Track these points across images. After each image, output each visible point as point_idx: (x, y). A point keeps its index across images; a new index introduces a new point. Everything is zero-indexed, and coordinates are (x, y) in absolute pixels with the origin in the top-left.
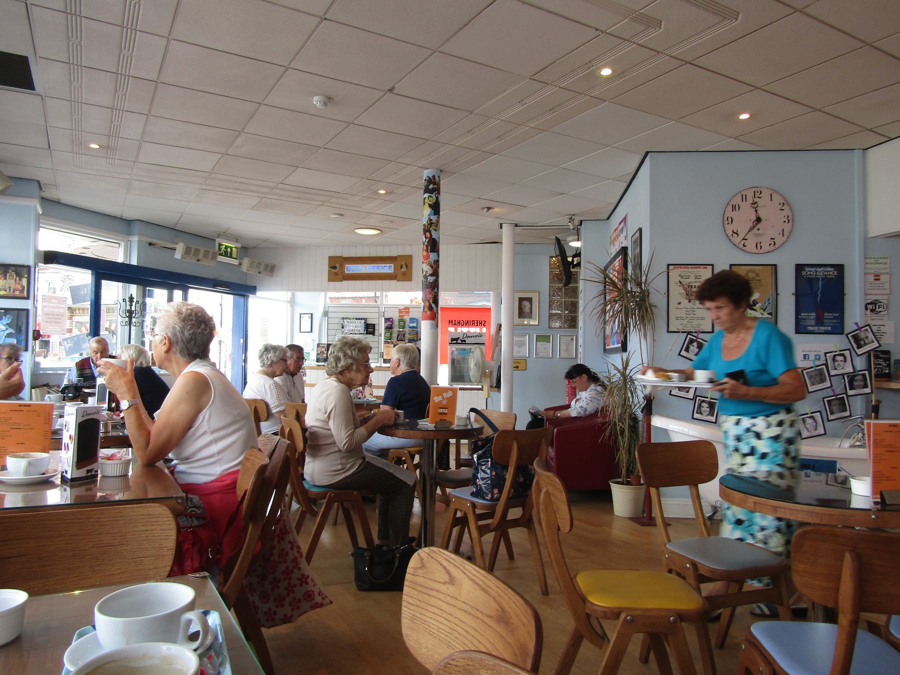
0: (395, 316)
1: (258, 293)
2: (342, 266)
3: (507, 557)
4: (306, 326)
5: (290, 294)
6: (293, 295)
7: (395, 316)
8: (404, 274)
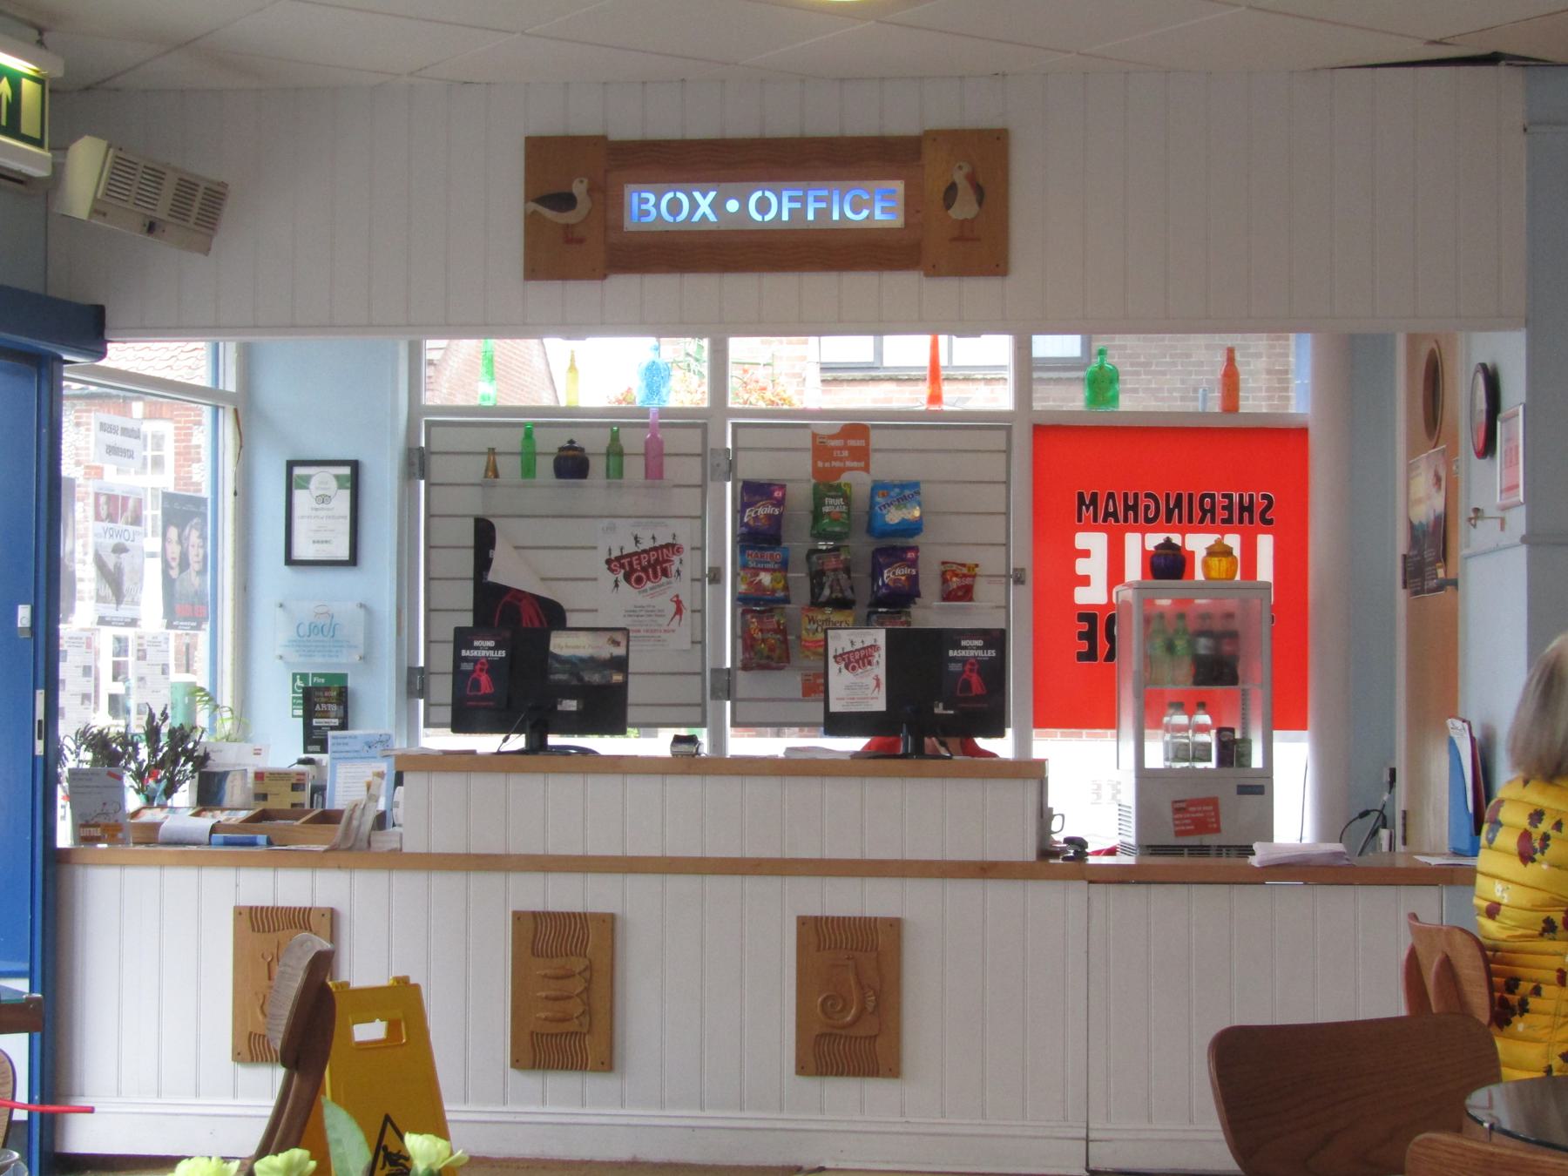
0: (797, 472)
1: (122, 355)
2: (608, 201)
3: (1446, 891)
4: (322, 532)
5: (925, 340)
6: (935, 347)
7: (797, 472)
8: (964, 234)
